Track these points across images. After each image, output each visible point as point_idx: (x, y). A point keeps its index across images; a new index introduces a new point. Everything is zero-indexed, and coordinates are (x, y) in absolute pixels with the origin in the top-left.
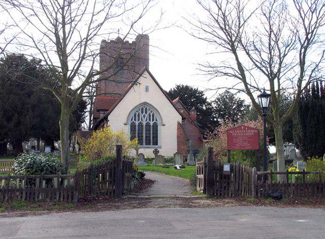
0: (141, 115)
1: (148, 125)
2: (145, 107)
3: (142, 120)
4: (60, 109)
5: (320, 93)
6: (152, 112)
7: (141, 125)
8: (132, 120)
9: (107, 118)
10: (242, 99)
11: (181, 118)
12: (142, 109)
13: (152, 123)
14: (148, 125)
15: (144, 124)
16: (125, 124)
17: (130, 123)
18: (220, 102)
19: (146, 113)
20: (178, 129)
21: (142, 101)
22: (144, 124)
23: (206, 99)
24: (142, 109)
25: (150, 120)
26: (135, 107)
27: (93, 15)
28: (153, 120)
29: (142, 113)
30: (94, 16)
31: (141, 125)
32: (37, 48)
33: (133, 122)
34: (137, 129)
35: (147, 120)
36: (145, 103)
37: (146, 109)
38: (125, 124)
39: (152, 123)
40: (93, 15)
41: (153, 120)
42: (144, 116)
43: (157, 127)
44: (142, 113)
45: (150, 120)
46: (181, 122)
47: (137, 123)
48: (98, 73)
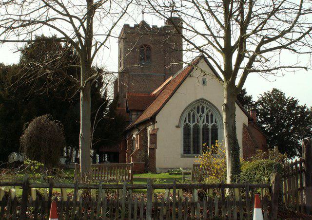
0: (197, 116)
1: (205, 128)
2: (201, 105)
3: (198, 122)
4: (91, 98)
5: (80, 164)
6: (209, 111)
7: (196, 128)
8: (185, 121)
9: (155, 118)
10: (294, 100)
11: (247, 119)
12: (198, 108)
13: (210, 126)
14: (205, 128)
15: (201, 126)
16: (177, 127)
17: (183, 125)
18: (266, 103)
19: (203, 112)
20: (243, 128)
21: (199, 98)
22: (201, 126)
23: (250, 98)
24: (198, 108)
25: (208, 122)
26: (191, 104)
27: (299, 14)
28: (212, 122)
29: (198, 112)
30: (301, 17)
31: (196, 128)
32: (204, 20)
33: (187, 124)
34: (192, 133)
35: (203, 122)
36: (202, 100)
37: (203, 108)
38: (177, 127)
39: (210, 126)
40: (299, 14)
41: (212, 122)
42: (201, 116)
43: (217, 130)
44: (198, 112)
45: (208, 122)
46: (247, 124)
47: (192, 125)
48: (33, 41)
